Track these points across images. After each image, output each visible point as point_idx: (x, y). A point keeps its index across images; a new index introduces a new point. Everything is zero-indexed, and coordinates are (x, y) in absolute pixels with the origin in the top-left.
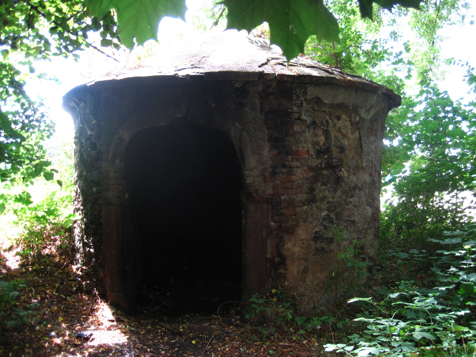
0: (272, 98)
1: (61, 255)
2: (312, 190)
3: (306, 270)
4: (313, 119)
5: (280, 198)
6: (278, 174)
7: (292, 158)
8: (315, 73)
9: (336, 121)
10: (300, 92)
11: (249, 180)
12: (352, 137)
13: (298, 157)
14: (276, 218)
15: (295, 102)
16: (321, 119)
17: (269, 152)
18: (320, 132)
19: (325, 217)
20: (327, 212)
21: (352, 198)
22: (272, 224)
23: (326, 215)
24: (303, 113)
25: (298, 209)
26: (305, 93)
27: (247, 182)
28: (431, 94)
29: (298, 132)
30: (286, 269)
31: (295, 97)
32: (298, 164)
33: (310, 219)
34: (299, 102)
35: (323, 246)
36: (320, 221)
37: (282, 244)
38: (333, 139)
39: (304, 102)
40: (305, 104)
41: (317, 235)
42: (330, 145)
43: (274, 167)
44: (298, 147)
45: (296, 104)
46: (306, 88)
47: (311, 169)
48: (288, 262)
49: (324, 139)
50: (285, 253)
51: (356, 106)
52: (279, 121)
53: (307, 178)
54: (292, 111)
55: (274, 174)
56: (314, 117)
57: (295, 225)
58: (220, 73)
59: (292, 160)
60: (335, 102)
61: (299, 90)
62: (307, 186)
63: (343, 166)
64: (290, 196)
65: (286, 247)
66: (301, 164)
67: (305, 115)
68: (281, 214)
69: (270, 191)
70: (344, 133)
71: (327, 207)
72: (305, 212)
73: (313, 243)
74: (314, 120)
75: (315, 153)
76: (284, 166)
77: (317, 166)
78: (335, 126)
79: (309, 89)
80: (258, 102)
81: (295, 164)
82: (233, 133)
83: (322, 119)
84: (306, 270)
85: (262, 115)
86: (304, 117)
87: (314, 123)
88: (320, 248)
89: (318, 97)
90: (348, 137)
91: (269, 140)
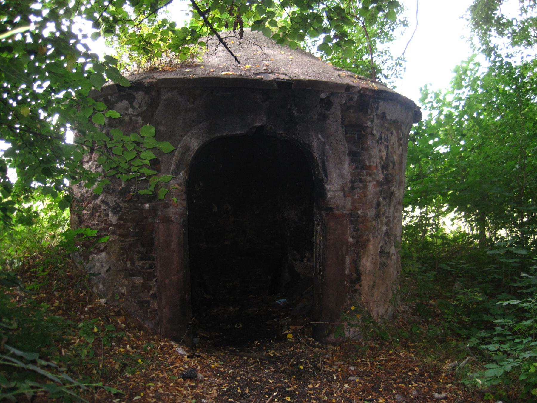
0: (352, 111)
1: (423, 265)
6: (356, 188)
18: (383, 148)
25: (369, 224)
28: (169, 40)
30: (360, 285)
40: (375, 120)
43: (352, 181)
46: (379, 103)
52: (356, 136)
55: (353, 188)
58: (310, 81)
66: (373, 179)
69: (349, 206)
79: (381, 104)
80: (340, 115)
81: (369, 178)
82: (315, 144)
85: (343, 128)
91: (349, 154)
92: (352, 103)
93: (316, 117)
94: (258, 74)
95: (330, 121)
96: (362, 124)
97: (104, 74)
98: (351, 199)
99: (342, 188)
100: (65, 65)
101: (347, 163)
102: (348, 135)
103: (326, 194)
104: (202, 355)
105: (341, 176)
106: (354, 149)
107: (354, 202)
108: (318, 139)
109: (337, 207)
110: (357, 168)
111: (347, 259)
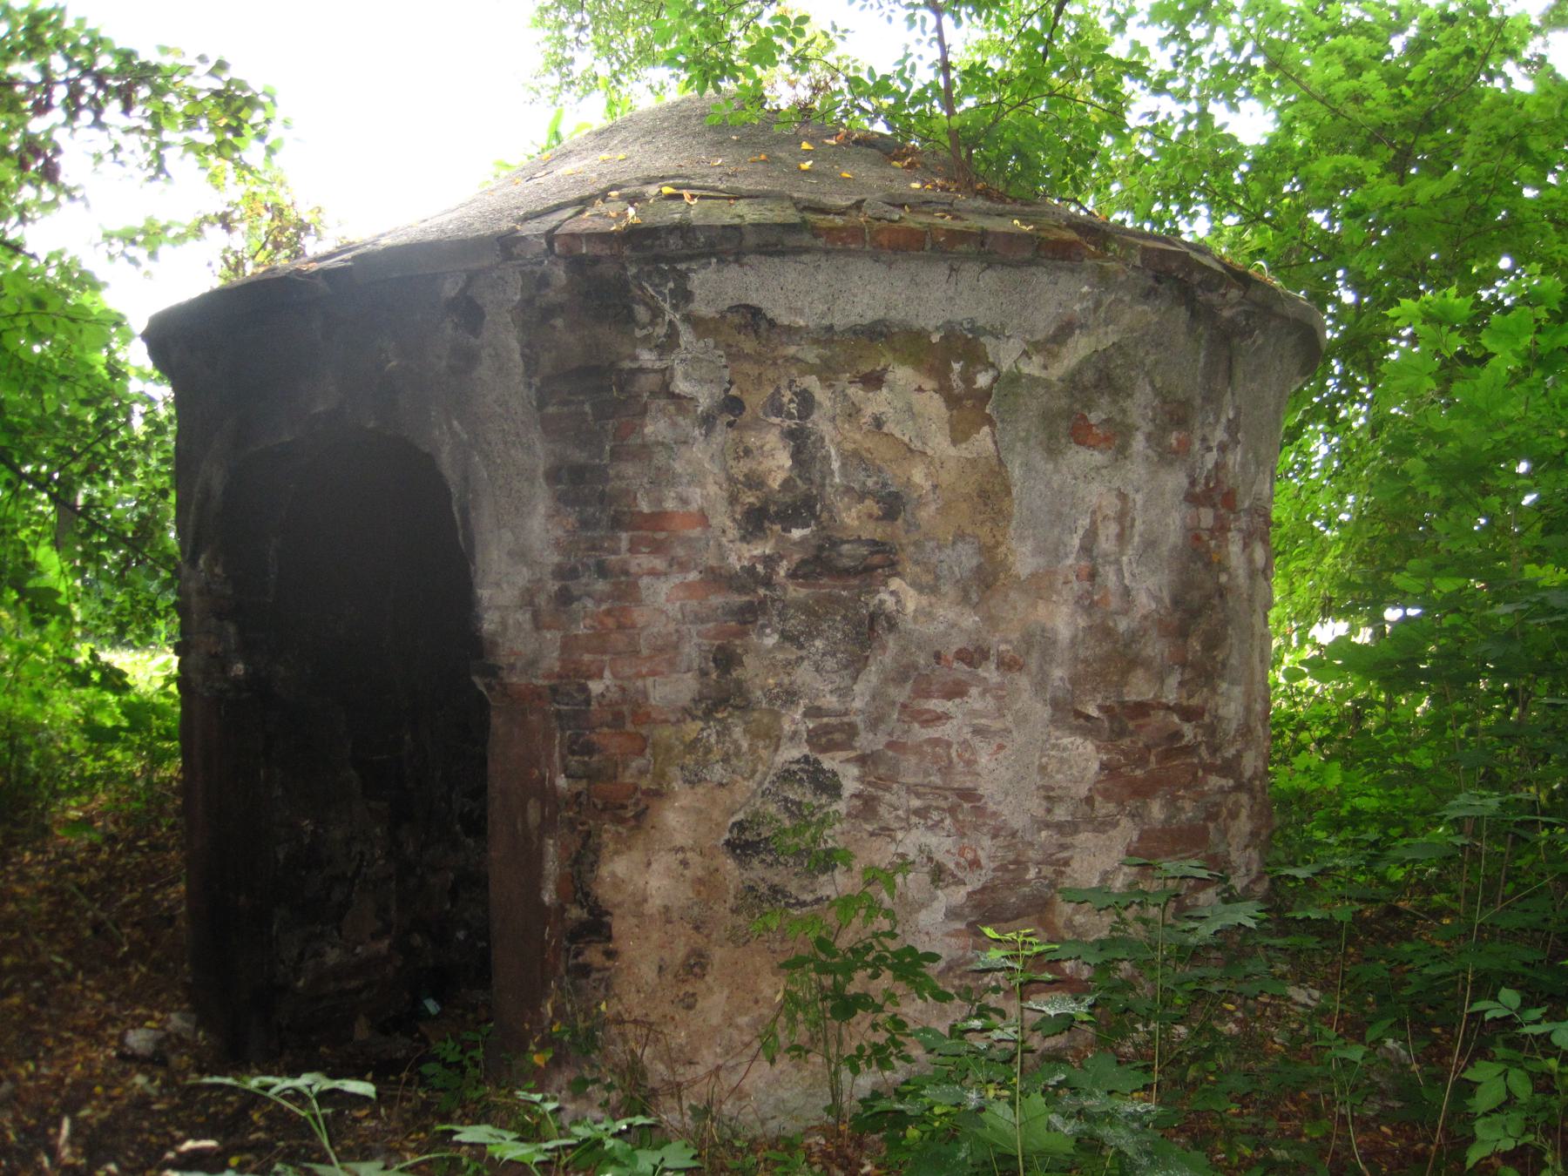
2: (725, 659)
3: (696, 964)
4: (727, 390)
5: (584, 689)
6: (579, 599)
7: (631, 541)
8: (748, 213)
9: (855, 392)
10: (660, 293)
11: (489, 624)
12: (952, 451)
13: (661, 535)
14: (573, 761)
15: (645, 332)
16: (771, 390)
17: (549, 517)
19: (795, 767)
20: (806, 750)
21: (958, 701)
22: (562, 782)
23: (798, 762)
24: (679, 370)
26: (683, 296)
27: (485, 626)
29: (663, 444)
31: (642, 313)
32: (659, 563)
33: (718, 772)
34: (661, 331)
35: (777, 880)
36: (766, 785)
37: (592, 857)
38: (836, 465)
39: (682, 328)
41: (749, 836)
42: (823, 485)
43: (565, 573)
44: (660, 501)
45: (647, 338)
46: (683, 276)
47: (718, 578)
48: (619, 926)
49: (788, 463)
50: (604, 893)
51: (970, 331)
53: (696, 615)
54: (634, 365)
55: (564, 598)
56: (731, 383)
57: (647, 793)
59: (633, 549)
60: (839, 321)
61: (654, 286)
62: (699, 645)
63: (899, 569)
64: (626, 684)
65: (604, 871)
67: (687, 376)
68: (589, 749)
70: (906, 439)
71: (809, 731)
72: (692, 746)
73: (730, 864)
74: (734, 392)
75: (734, 520)
76: (602, 571)
77: (751, 571)
78: (853, 412)
80: (515, 345)
83: (778, 390)
84: (696, 964)
85: (529, 385)
86: (682, 386)
87: (733, 405)
88: (763, 889)
89: (747, 307)
90: (930, 452)
91: (553, 476)
92: (551, 296)
93: (444, 363)
94: (584, 202)
95: (484, 371)
96: (612, 364)
97: (66, 1124)
98: (558, 635)
99: (528, 598)
100: (1413, 171)
101: (541, 509)
102: (551, 410)
103: (479, 618)
104: (74, 889)
105: (520, 555)
106: (580, 456)
107: (568, 645)
108: (454, 434)
109: (512, 667)
110: (585, 524)
111: (550, 846)
